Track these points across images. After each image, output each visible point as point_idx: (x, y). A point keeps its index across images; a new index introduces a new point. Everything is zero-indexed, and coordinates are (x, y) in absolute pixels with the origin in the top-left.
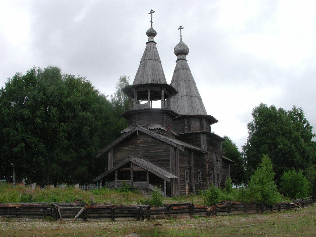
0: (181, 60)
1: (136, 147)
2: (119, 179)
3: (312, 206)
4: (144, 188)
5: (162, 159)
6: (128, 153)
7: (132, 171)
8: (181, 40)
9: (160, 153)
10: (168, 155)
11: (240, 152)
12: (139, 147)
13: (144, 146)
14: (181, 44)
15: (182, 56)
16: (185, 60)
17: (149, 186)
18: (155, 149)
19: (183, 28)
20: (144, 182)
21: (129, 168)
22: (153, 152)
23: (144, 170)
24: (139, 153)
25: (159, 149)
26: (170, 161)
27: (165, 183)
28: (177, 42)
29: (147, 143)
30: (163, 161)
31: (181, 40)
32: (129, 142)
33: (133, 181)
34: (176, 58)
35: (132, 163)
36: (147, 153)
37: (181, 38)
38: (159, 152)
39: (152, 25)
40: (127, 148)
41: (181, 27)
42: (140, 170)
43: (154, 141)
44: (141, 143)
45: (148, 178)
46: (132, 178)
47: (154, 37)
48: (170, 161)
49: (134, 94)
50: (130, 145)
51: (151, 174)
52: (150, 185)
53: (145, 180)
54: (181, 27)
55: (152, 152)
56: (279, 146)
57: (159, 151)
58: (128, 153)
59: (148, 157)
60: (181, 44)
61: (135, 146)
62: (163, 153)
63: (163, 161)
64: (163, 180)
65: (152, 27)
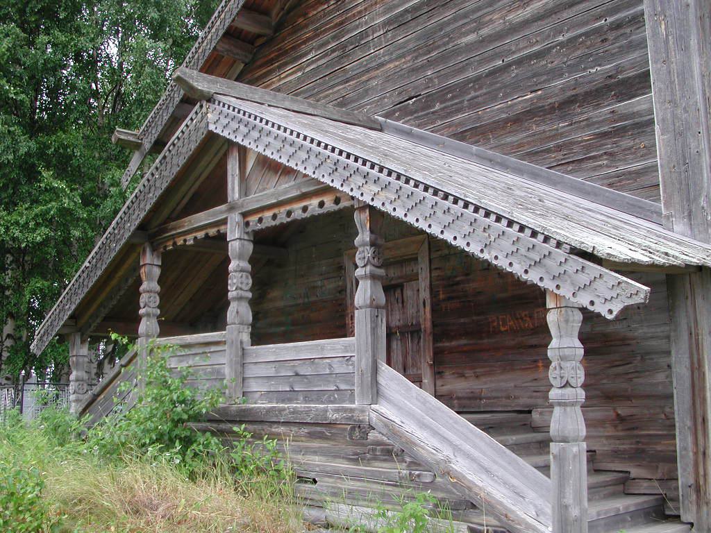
2: (170, 325)
4: (331, 411)
5: (559, 83)
7: (238, 245)
9: (534, 28)
10: (617, 26)
17: (376, 392)
20: (331, 347)
22: (469, 47)
23: (328, 200)
26: (641, 83)
27: (564, 345)
30: (565, 106)
35: (243, 151)
36: (423, 68)
38: (526, 23)
45: (364, 293)
46: (239, 312)
51: (402, 246)
52: (390, 377)
53: (338, 325)
56: (372, 435)
59: (429, 100)
61: (335, 38)
63: (571, 101)
64: (533, 298)
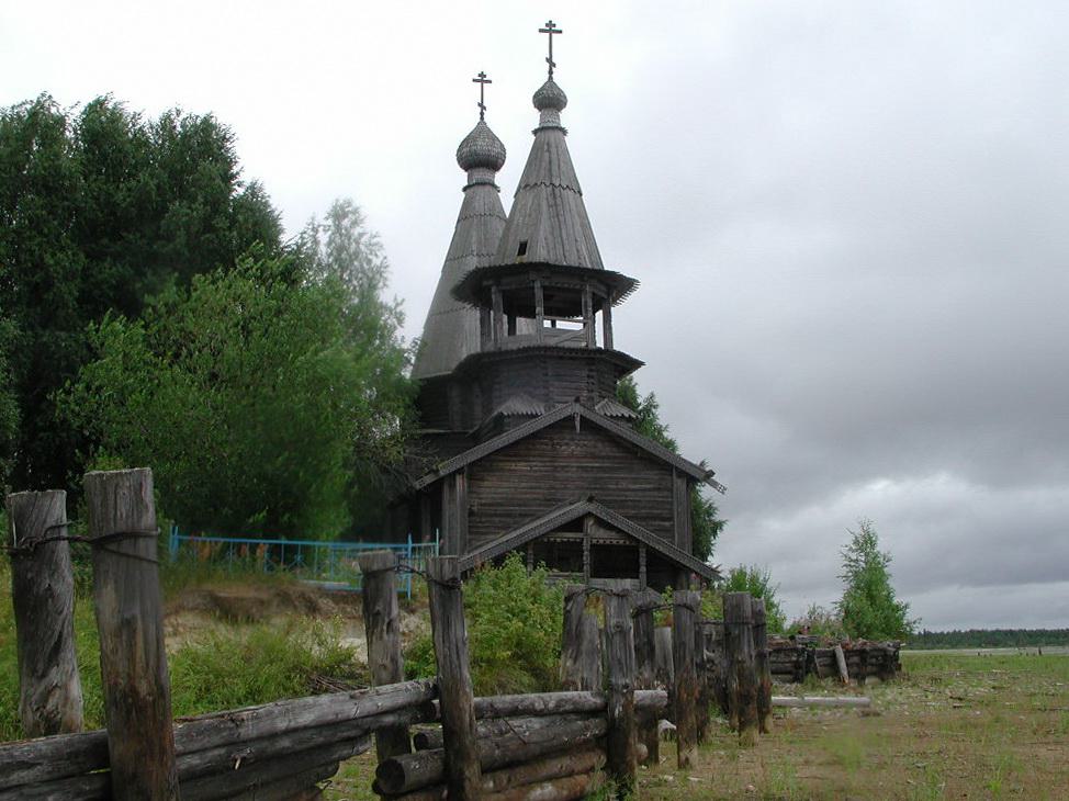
0: (476, 188)
1: (556, 467)
3: (272, 563)
6: (524, 485)
7: (586, 546)
8: (482, 118)
11: (702, 489)
12: (567, 467)
13: (582, 467)
14: (482, 130)
15: (481, 174)
16: (493, 186)
18: (623, 478)
19: (490, 82)
21: (580, 535)
22: (614, 490)
24: (565, 488)
25: (635, 480)
28: (469, 125)
29: (594, 457)
31: (482, 118)
32: (531, 447)
33: (591, 577)
34: (462, 178)
37: (482, 114)
38: (634, 490)
39: (551, 72)
40: (522, 466)
41: (482, 75)
42: (615, 542)
43: (617, 455)
44: (571, 456)
47: (559, 110)
48: (670, 519)
49: (493, 296)
50: (531, 459)
54: (482, 75)
55: (609, 489)
57: (637, 486)
58: (524, 485)
60: (482, 130)
62: (648, 493)
65: (551, 78)
